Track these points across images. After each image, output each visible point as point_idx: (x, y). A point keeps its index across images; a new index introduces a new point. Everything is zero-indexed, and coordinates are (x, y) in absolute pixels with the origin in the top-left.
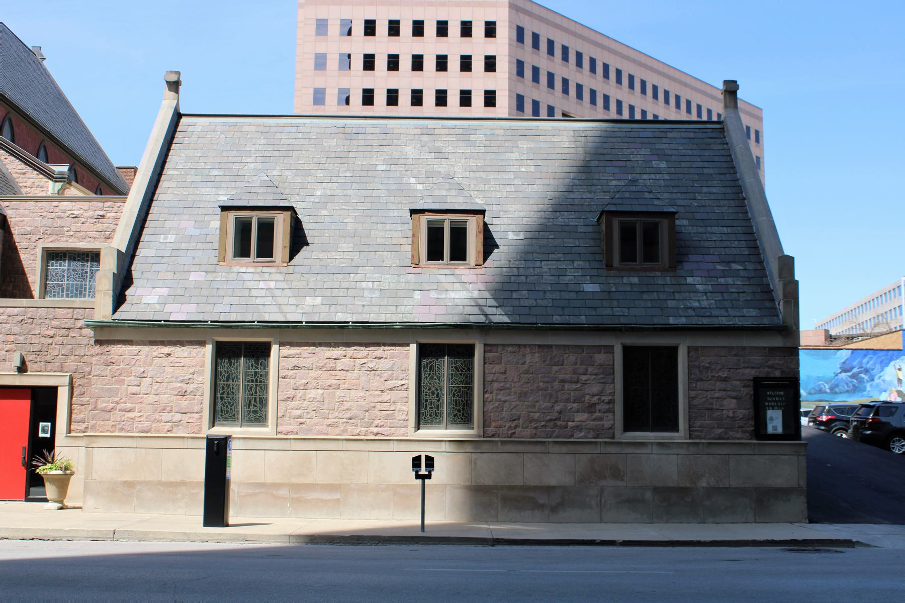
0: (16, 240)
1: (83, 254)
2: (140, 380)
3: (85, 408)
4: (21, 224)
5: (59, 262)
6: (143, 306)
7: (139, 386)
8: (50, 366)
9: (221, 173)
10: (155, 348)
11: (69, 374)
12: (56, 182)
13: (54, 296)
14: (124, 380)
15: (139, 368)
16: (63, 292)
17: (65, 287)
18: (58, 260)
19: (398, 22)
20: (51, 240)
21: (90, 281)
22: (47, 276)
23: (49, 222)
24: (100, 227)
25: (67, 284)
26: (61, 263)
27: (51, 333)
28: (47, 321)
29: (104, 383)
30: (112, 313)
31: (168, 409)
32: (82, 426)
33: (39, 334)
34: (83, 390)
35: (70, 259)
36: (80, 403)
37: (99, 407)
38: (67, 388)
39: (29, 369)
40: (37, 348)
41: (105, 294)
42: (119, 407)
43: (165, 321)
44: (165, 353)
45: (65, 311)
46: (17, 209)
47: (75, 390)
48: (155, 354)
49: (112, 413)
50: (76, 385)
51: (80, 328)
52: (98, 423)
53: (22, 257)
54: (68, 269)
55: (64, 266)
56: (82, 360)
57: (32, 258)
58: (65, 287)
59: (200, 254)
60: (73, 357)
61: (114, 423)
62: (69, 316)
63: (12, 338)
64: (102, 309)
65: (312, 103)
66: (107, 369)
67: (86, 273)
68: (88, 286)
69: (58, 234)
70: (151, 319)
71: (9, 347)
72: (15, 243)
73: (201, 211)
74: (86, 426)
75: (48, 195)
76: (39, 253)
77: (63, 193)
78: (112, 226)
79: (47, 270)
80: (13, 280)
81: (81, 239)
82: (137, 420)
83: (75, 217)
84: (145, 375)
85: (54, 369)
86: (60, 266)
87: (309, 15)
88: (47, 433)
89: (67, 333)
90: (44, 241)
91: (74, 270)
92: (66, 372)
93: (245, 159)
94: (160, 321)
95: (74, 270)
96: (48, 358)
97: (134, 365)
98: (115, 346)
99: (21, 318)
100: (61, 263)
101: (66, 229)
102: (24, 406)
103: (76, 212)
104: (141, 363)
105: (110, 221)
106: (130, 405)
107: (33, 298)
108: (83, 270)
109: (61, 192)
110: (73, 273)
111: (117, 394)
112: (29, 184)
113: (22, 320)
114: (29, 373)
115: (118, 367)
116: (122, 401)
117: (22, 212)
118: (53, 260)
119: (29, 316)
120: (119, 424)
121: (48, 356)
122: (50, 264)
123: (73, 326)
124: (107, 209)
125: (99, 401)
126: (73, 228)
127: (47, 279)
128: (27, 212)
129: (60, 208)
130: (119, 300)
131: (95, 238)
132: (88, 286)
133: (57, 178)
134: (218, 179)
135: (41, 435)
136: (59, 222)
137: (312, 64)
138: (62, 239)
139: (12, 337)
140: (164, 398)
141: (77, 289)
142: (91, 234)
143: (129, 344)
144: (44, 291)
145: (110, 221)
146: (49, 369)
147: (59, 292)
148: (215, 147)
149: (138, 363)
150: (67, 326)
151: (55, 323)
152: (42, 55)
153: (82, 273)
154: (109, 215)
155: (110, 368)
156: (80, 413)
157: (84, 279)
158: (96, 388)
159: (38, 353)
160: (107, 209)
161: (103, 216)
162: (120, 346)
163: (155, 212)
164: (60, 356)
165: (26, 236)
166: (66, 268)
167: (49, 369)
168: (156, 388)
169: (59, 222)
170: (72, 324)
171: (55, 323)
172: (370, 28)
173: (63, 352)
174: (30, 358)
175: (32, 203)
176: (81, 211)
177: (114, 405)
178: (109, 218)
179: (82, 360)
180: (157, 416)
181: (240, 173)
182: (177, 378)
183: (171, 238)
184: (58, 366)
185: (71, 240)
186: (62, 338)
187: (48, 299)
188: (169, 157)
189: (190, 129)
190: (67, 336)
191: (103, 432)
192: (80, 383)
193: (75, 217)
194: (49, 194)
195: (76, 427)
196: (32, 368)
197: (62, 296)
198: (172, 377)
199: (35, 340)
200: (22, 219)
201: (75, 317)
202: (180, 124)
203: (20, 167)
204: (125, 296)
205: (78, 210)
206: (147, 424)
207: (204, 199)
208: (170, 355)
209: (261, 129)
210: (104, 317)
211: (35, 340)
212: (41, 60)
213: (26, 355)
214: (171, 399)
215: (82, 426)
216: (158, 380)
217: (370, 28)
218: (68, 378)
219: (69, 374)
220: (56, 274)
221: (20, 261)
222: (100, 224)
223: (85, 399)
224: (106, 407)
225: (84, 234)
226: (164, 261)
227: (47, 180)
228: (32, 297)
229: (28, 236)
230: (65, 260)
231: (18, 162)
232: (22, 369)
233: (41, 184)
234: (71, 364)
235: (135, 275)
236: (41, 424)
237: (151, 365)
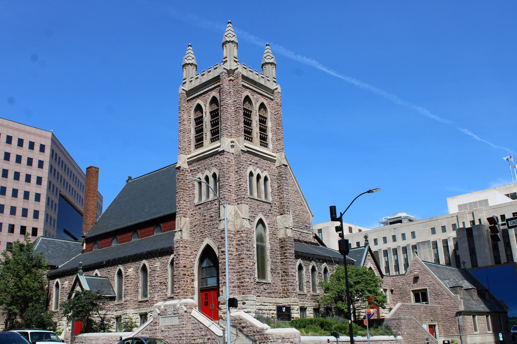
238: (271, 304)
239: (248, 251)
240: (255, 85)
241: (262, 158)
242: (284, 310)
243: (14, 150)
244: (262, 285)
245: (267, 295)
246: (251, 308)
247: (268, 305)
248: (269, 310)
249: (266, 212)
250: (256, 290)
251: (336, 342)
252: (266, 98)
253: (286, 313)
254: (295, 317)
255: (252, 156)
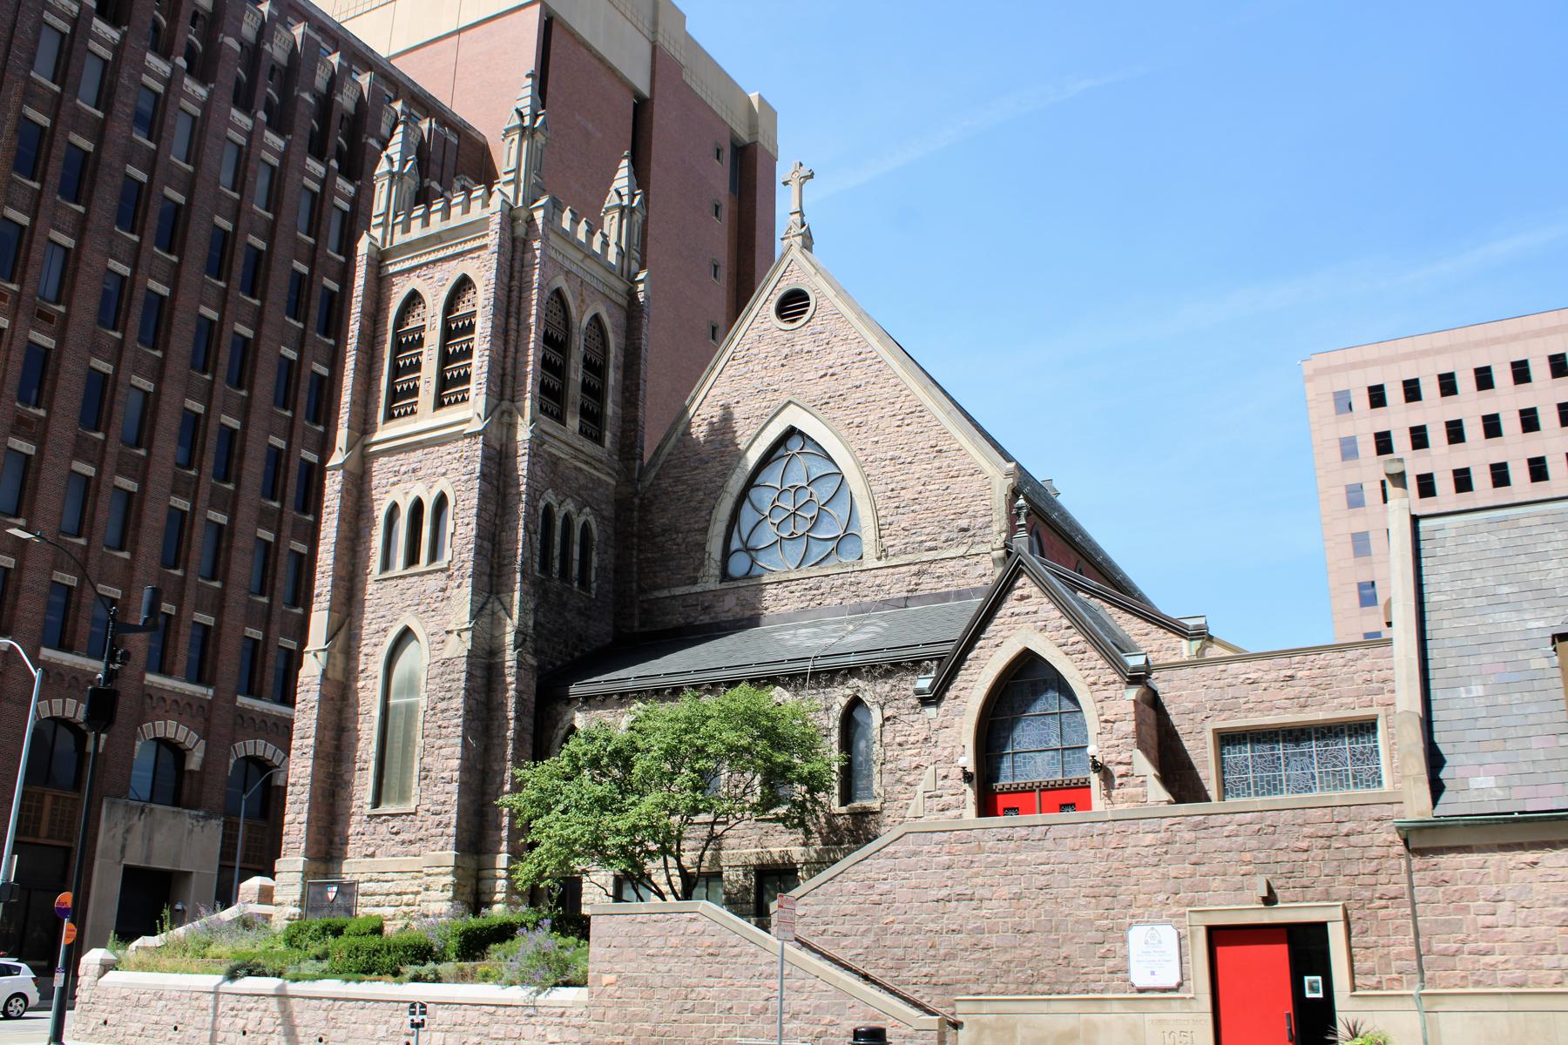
0: (1174, 723)
1: (1270, 733)
2: (1494, 906)
3: (1373, 953)
4: (1178, 700)
5: (1238, 747)
6: (1476, 793)
7: (1494, 914)
8: (1309, 893)
9: (1515, 589)
10: (1509, 855)
11: (1341, 903)
12: (1191, 640)
13: (1238, 795)
14: (1468, 906)
15: (1489, 887)
16: (1249, 788)
17: (1251, 781)
18: (1235, 745)
19: (1416, 381)
20: (1223, 717)
21: (1286, 770)
22: (1223, 768)
23: (1216, 694)
24: (1289, 692)
25: (1254, 777)
26: (1240, 749)
27: (1304, 845)
28: (1296, 828)
29: (1437, 912)
30: (1431, 806)
31: (1550, 948)
32: (1373, 980)
33: (1287, 847)
34: (1365, 926)
35: (1252, 741)
36: (1363, 945)
37: (1434, 949)
38: (1342, 923)
39: (1279, 899)
40: (1286, 867)
41: (1415, 780)
42: (1466, 948)
43: (1520, 813)
44: (1529, 861)
45: (1320, 812)
46: (1170, 681)
47: (1352, 926)
48: (1512, 863)
49: (1457, 958)
50: (1352, 919)
51: (1347, 835)
52: (1438, 974)
53: (1186, 745)
54: (1252, 756)
55: (1246, 752)
56: (1357, 882)
57: (1201, 745)
58: (1251, 781)
59: (1533, 709)
60: (1341, 878)
61: (1463, 974)
62: (1327, 818)
63: (1248, 856)
64: (1417, 806)
65: (1346, 507)
66: (1437, 891)
67: (1279, 758)
68: (1284, 778)
69: (1232, 709)
70: (1496, 811)
71: (1245, 869)
72: (1173, 726)
73: (1507, 647)
74: (1377, 979)
75: (1182, 660)
76: (1209, 738)
77: (1203, 655)
78: (1307, 689)
79: (1222, 760)
80: (1178, 777)
81: (1266, 713)
82: (1501, 968)
83: (1253, 683)
84: (1501, 897)
85: (1317, 897)
86: (1240, 753)
87: (1319, 394)
88: (1318, 992)
89: (1328, 843)
90: (1213, 721)
91: (1261, 757)
92: (1336, 900)
93: (1542, 565)
94: (1512, 813)
95: (1261, 757)
96: (1305, 881)
97: (1480, 883)
98: (1445, 857)
99: (1257, 827)
100: (1240, 749)
101: (1242, 701)
102: (1279, 953)
103: (1253, 676)
104: (1492, 879)
105: (1303, 682)
106: (1485, 944)
107: (1210, 801)
108: (1273, 755)
109: (1199, 653)
110: (1259, 760)
111: (1461, 927)
112: (1155, 648)
113: (1259, 830)
114: (1279, 905)
115: (1455, 888)
116: (1471, 939)
117: (1177, 683)
118: (1228, 745)
119: (1269, 822)
120: (1472, 974)
121: (1305, 879)
122: (1225, 751)
123: (1335, 833)
124: (1296, 666)
125: (1434, 941)
126: (1252, 698)
127: (1224, 773)
128: (1184, 683)
129: (1229, 672)
130: (1437, 789)
131: (1285, 708)
132: (1284, 778)
133: (1192, 635)
134: (1512, 598)
135: (1309, 995)
136: (1230, 692)
137: (1337, 453)
138: (1239, 715)
139: (1248, 854)
140: (1540, 931)
141: (1268, 783)
142: (1278, 703)
143: (1466, 852)
144: (1224, 792)
145: (1303, 682)
146: (1308, 897)
147: (1243, 789)
148: (1488, 554)
149: (1486, 880)
150: (1326, 833)
151: (1307, 830)
152: (1055, 490)
153: (1273, 760)
154: (1299, 674)
155: (1442, 889)
156: (1366, 960)
157: (1276, 768)
158: (1426, 921)
159: (1290, 875)
160: (1296, 666)
161: (1292, 677)
162: (1452, 855)
163: (1435, 656)
164: (1323, 877)
165: (1187, 716)
166: (1249, 755)
167: (1308, 897)
168: (1523, 917)
169: (1230, 692)
170: (1333, 829)
171: (1307, 830)
172: (1377, 397)
173: (1326, 872)
174: (1280, 883)
175: (1189, 670)
176: (1260, 674)
177: (1458, 945)
178: (1301, 678)
179: (1357, 882)
180: (1533, 960)
181: (1545, 585)
182: (1555, 898)
183: (1478, 690)
184: (1322, 892)
185: (1252, 714)
186: (1320, 851)
187: (1229, 800)
188: (1424, 578)
189: (1438, 535)
190: (1329, 847)
191: (1449, 988)
192: (1359, 916)
193: (1253, 683)
194: (1185, 658)
195: (1363, 982)
196: (1283, 897)
197: (1249, 794)
198: (1547, 898)
199: (1282, 856)
200: (1179, 693)
201: (1336, 820)
202: (1421, 530)
203: (1139, 626)
204: (1440, 780)
205: (1256, 672)
206: (1518, 973)
207: (1503, 630)
208: (1536, 863)
209: (1550, 519)
210: (1419, 814)
211: (1282, 856)
212: (1054, 496)
213: (1272, 878)
214: (1552, 933)
215: (1373, 980)
216: (1524, 904)
217: (1377, 397)
218: (1340, 910)
219: (1341, 903)
220: (1236, 764)
221: (1185, 751)
222: (1289, 689)
223: (1371, 939)
224: (1446, 949)
225: (1268, 704)
226: (1481, 723)
227: (1179, 639)
228: (1208, 800)
229: (1191, 716)
230: (1245, 744)
231: (1136, 620)
232: (1270, 900)
233: (1173, 645)
234: (1341, 887)
235: (1443, 749)
236: (1307, 978)
237: (1507, 881)
238: (405, 876)
239: (302, 738)
240: (441, 243)
241: (433, 446)
242: (331, 896)
243: (1398, 418)
244: (385, 821)
245: (399, 849)
246: (284, 892)
247: (393, 881)
248: (399, 894)
249: (428, 601)
250: (364, 838)
251: (212, 996)
252: (475, 255)
253: (340, 901)
254: (430, 913)
255: (402, 456)
